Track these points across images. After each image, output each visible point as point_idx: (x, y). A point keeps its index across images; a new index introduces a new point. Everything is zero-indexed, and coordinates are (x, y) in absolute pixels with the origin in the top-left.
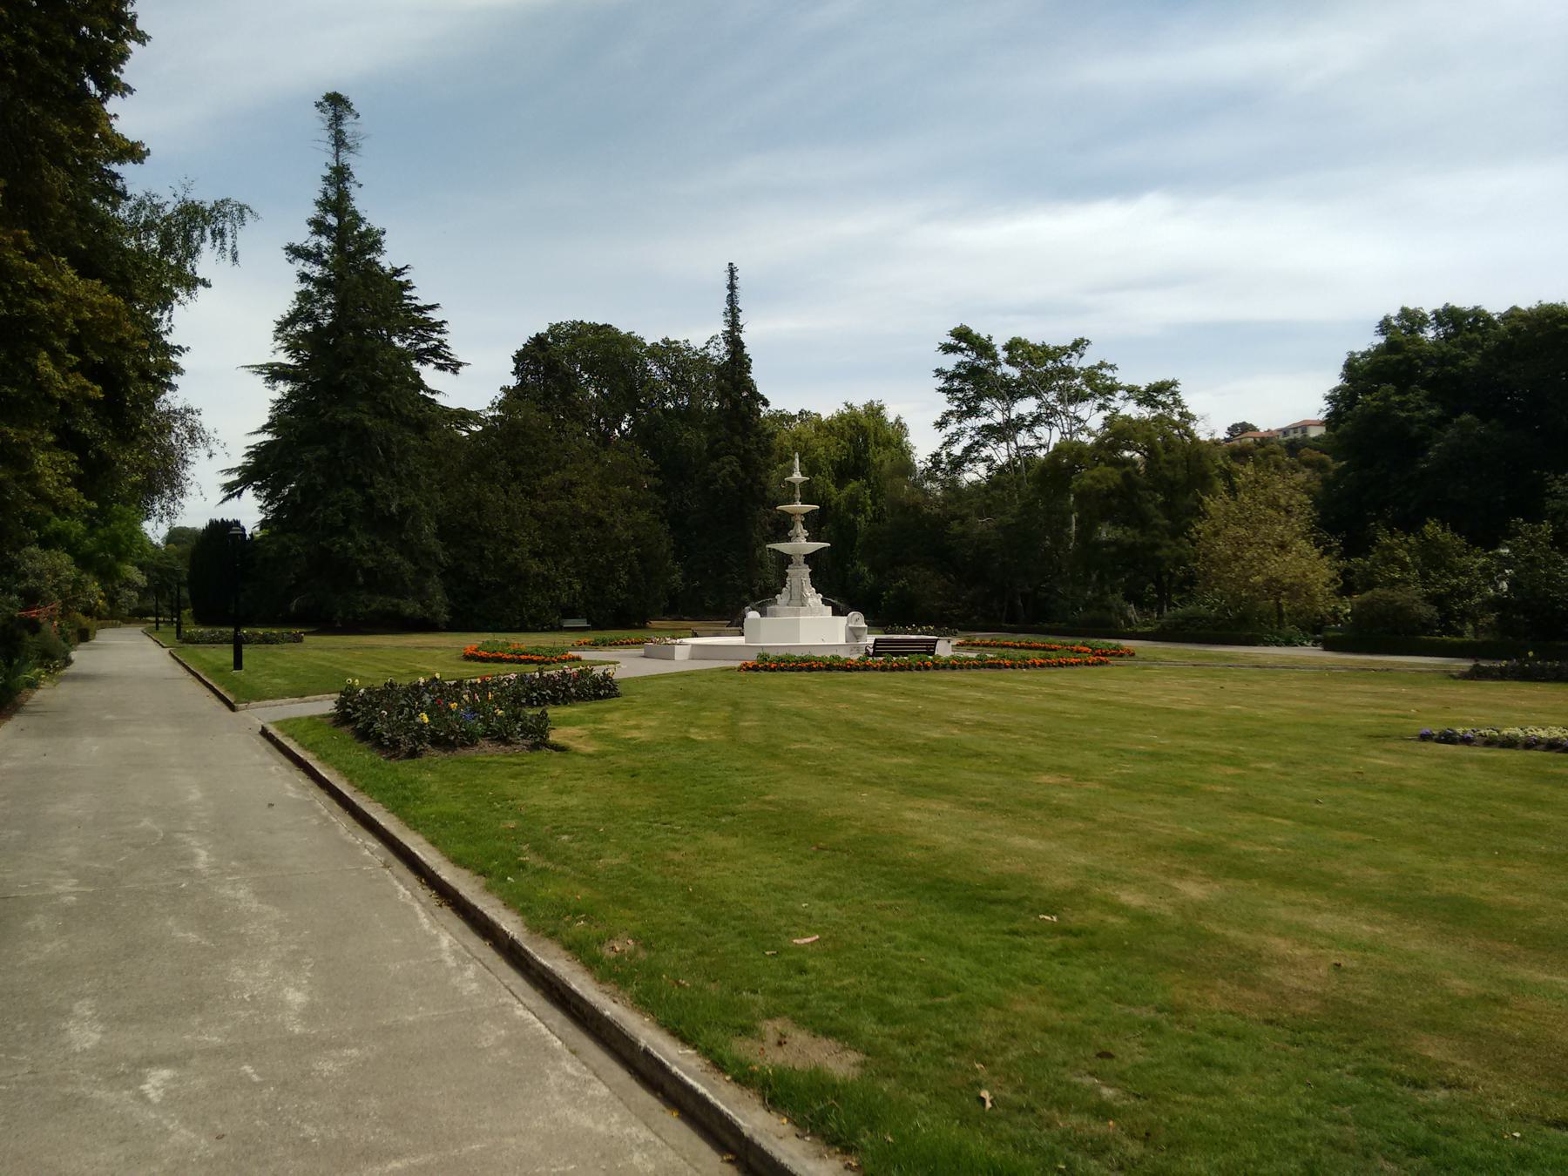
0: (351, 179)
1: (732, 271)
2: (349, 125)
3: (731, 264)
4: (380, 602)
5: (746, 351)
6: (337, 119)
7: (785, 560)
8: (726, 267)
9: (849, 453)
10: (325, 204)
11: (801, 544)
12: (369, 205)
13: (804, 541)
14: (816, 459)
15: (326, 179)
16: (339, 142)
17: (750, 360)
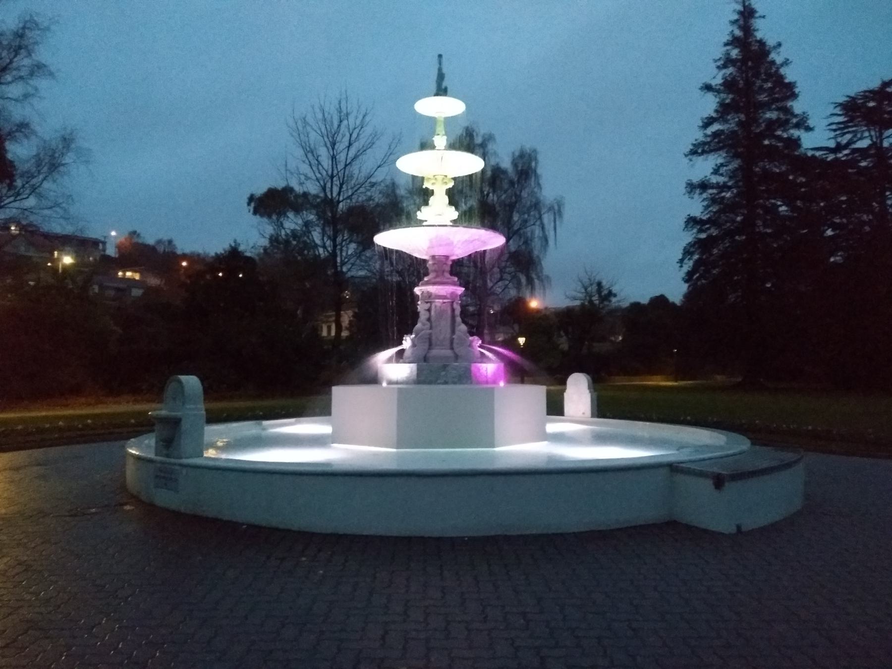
10: (734, 42)
12: (764, 31)
15: (736, 21)
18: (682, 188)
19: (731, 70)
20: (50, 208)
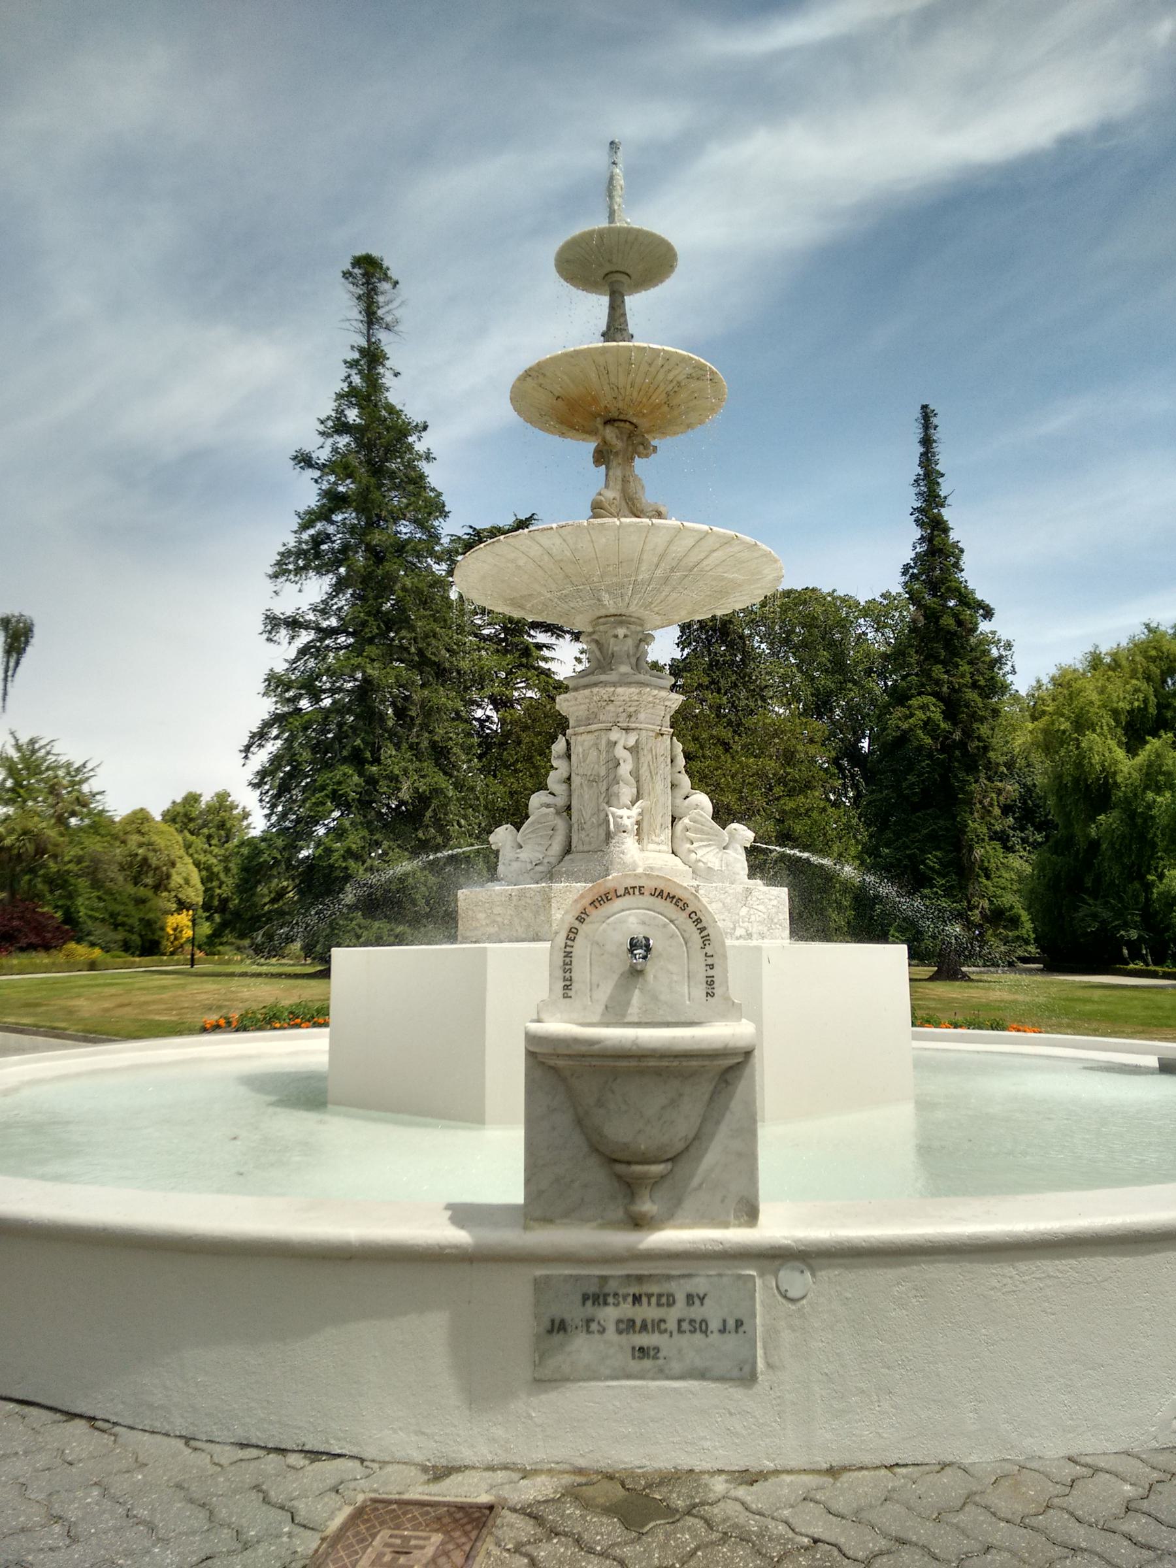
0: (388, 363)
1: (927, 415)
3: (925, 407)
5: (953, 536)
8: (917, 413)
9: (1146, 701)
10: (350, 395)
16: (371, 317)
17: (962, 551)
19: (343, 441)
20: (671, 897)
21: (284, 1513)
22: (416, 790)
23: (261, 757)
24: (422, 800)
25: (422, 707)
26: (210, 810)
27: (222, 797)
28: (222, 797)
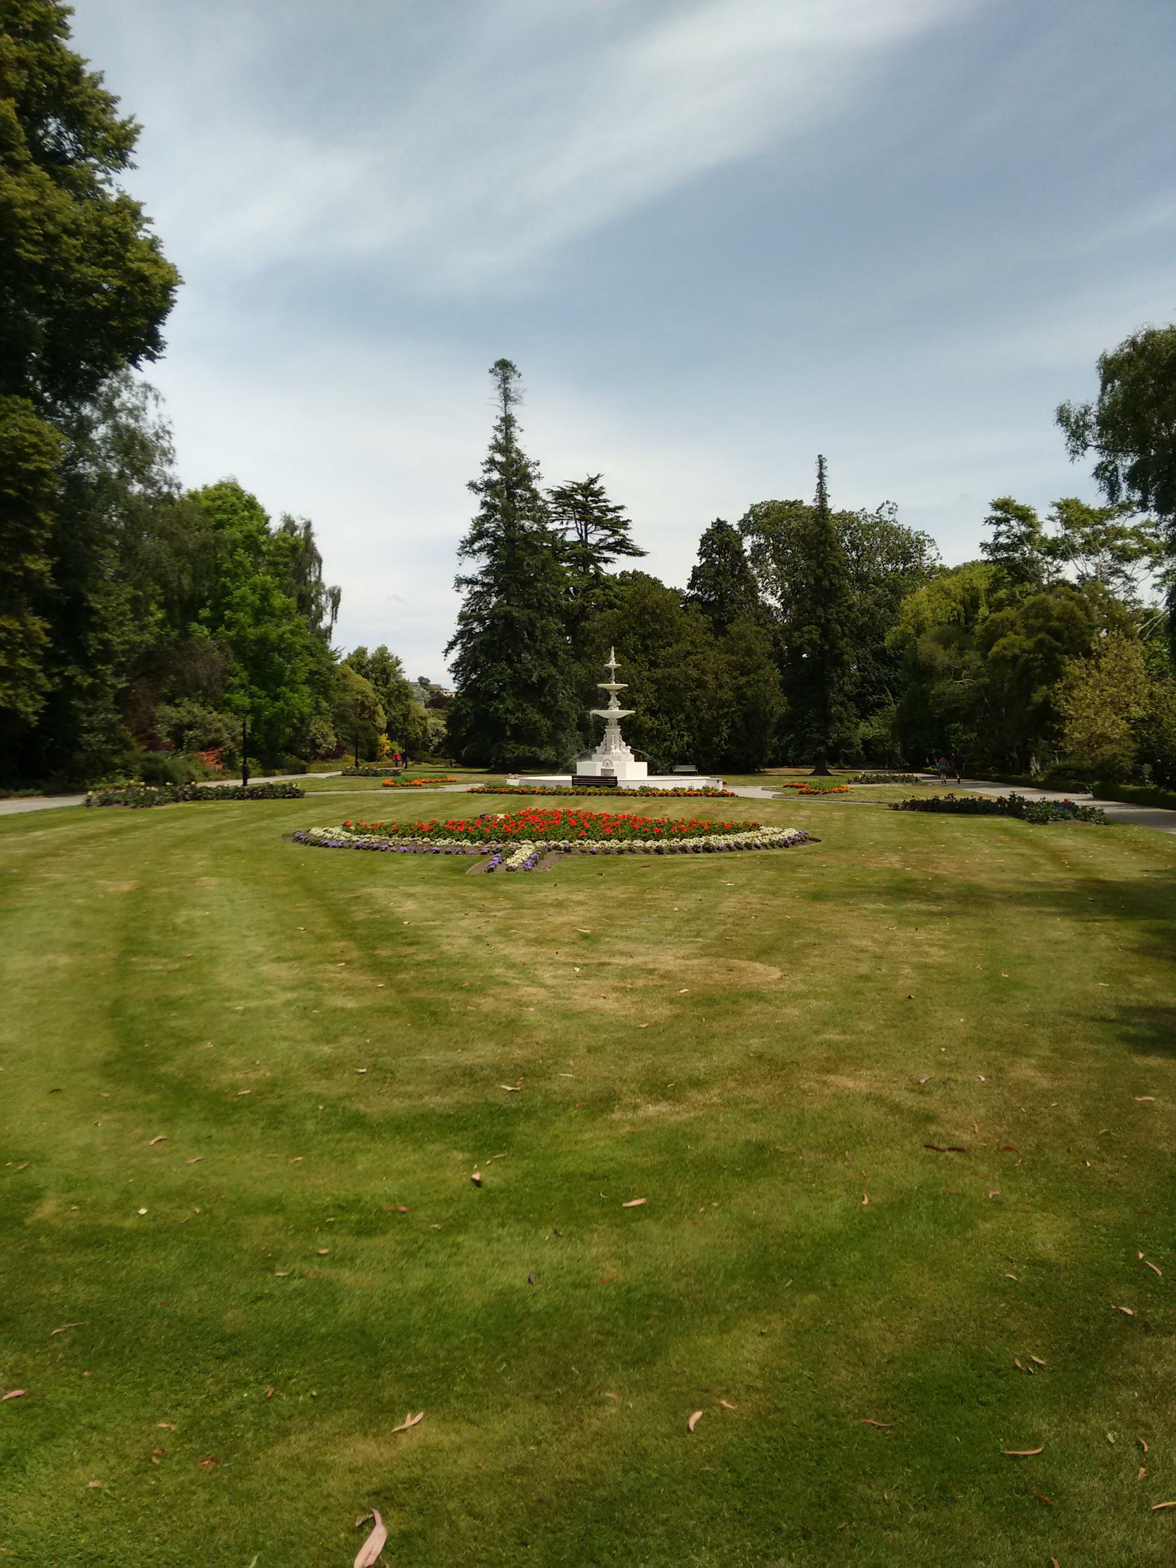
1: (821, 460)
2: (513, 384)
4: (523, 750)
6: (505, 380)
7: (602, 723)
8: (817, 460)
9: (959, 615)
10: (497, 448)
11: (615, 711)
12: (526, 443)
13: (617, 710)
14: (923, 621)
15: (496, 429)
16: (507, 397)
18: (453, 583)
21: (546, 862)
22: (540, 676)
23: (455, 655)
24: (543, 681)
25: (542, 630)
26: (374, 660)
27: (382, 651)
28: (382, 651)
